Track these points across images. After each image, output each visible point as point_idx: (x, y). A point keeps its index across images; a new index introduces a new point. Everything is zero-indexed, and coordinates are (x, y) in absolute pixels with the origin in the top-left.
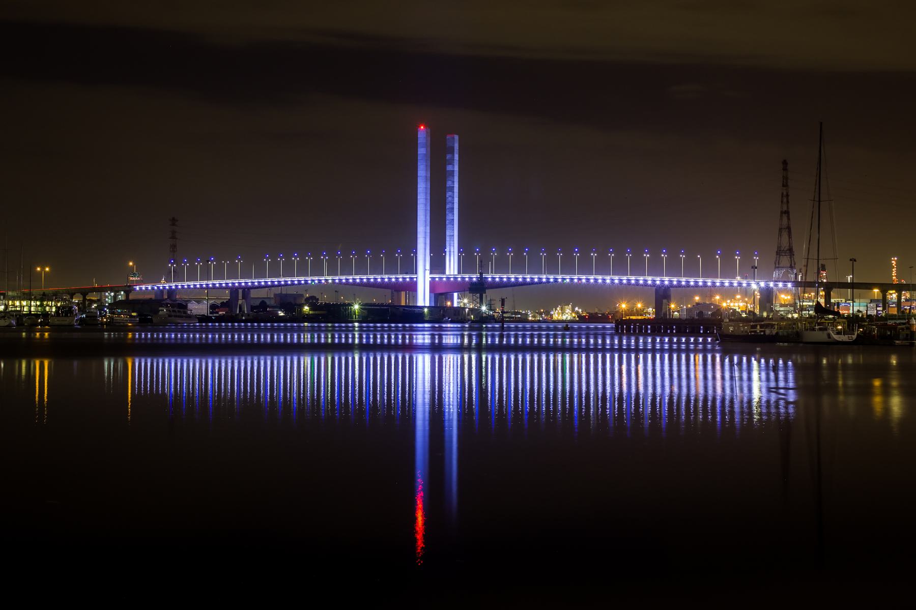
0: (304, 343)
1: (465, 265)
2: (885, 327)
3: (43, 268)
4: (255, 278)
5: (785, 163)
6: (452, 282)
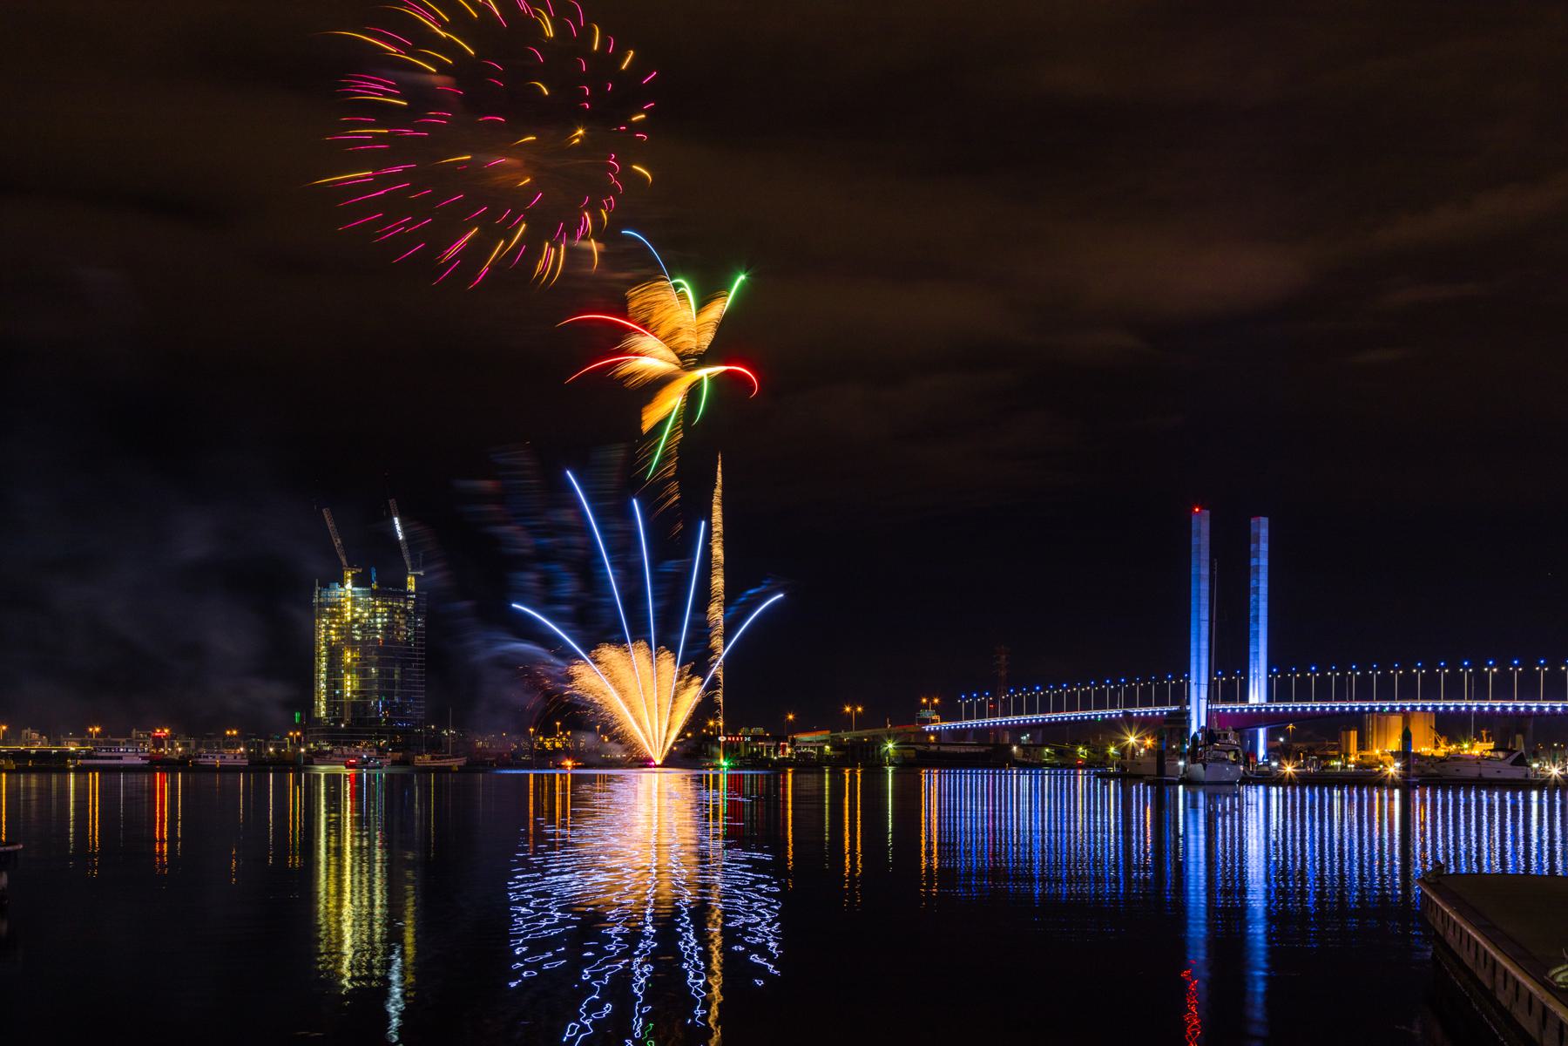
1: (1277, 690)
3: (854, 708)
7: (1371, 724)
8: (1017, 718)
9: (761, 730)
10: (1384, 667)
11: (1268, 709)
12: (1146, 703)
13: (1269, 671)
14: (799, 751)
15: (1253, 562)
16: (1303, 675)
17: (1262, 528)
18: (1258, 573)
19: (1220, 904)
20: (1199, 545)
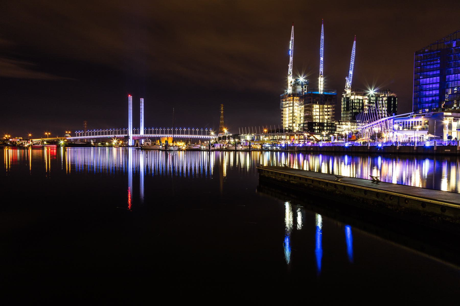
0: (281, 167)
1: (146, 132)
2: (308, 132)
5: (293, 22)
7: (161, 139)
8: (90, 136)
9: (21, 138)
10: (166, 128)
11: (144, 136)
12: (119, 134)
13: (144, 128)
14: (33, 143)
15: (141, 107)
16: (151, 129)
17: (142, 100)
18: (142, 109)
19: (185, 177)
20: (130, 103)
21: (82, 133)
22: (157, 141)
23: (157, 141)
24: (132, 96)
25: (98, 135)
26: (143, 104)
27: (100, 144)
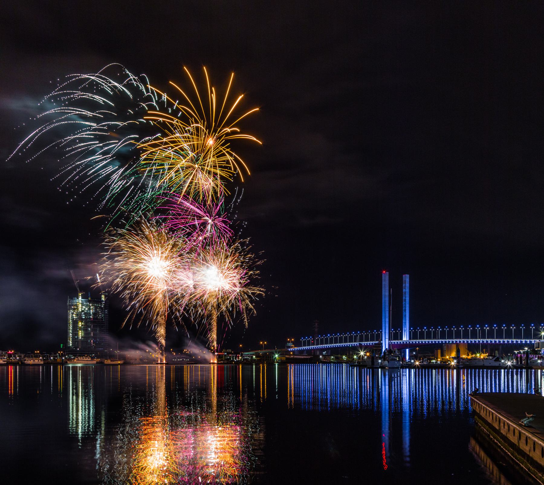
1: (413, 336)
3: (264, 342)
4: (505, 338)
6: (441, 343)
13: (410, 329)
15: (404, 290)
16: (422, 330)
17: (406, 278)
20: (385, 285)
21: (323, 338)
22: (436, 351)
23: (436, 351)
24: (388, 273)
25: (330, 344)
26: (408, 285)
27: (333, 359)
